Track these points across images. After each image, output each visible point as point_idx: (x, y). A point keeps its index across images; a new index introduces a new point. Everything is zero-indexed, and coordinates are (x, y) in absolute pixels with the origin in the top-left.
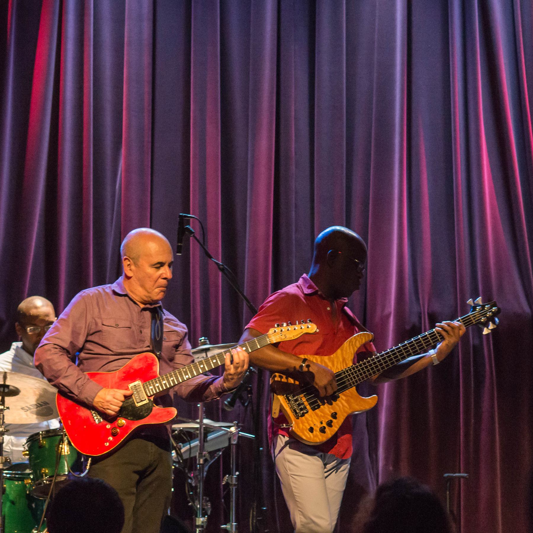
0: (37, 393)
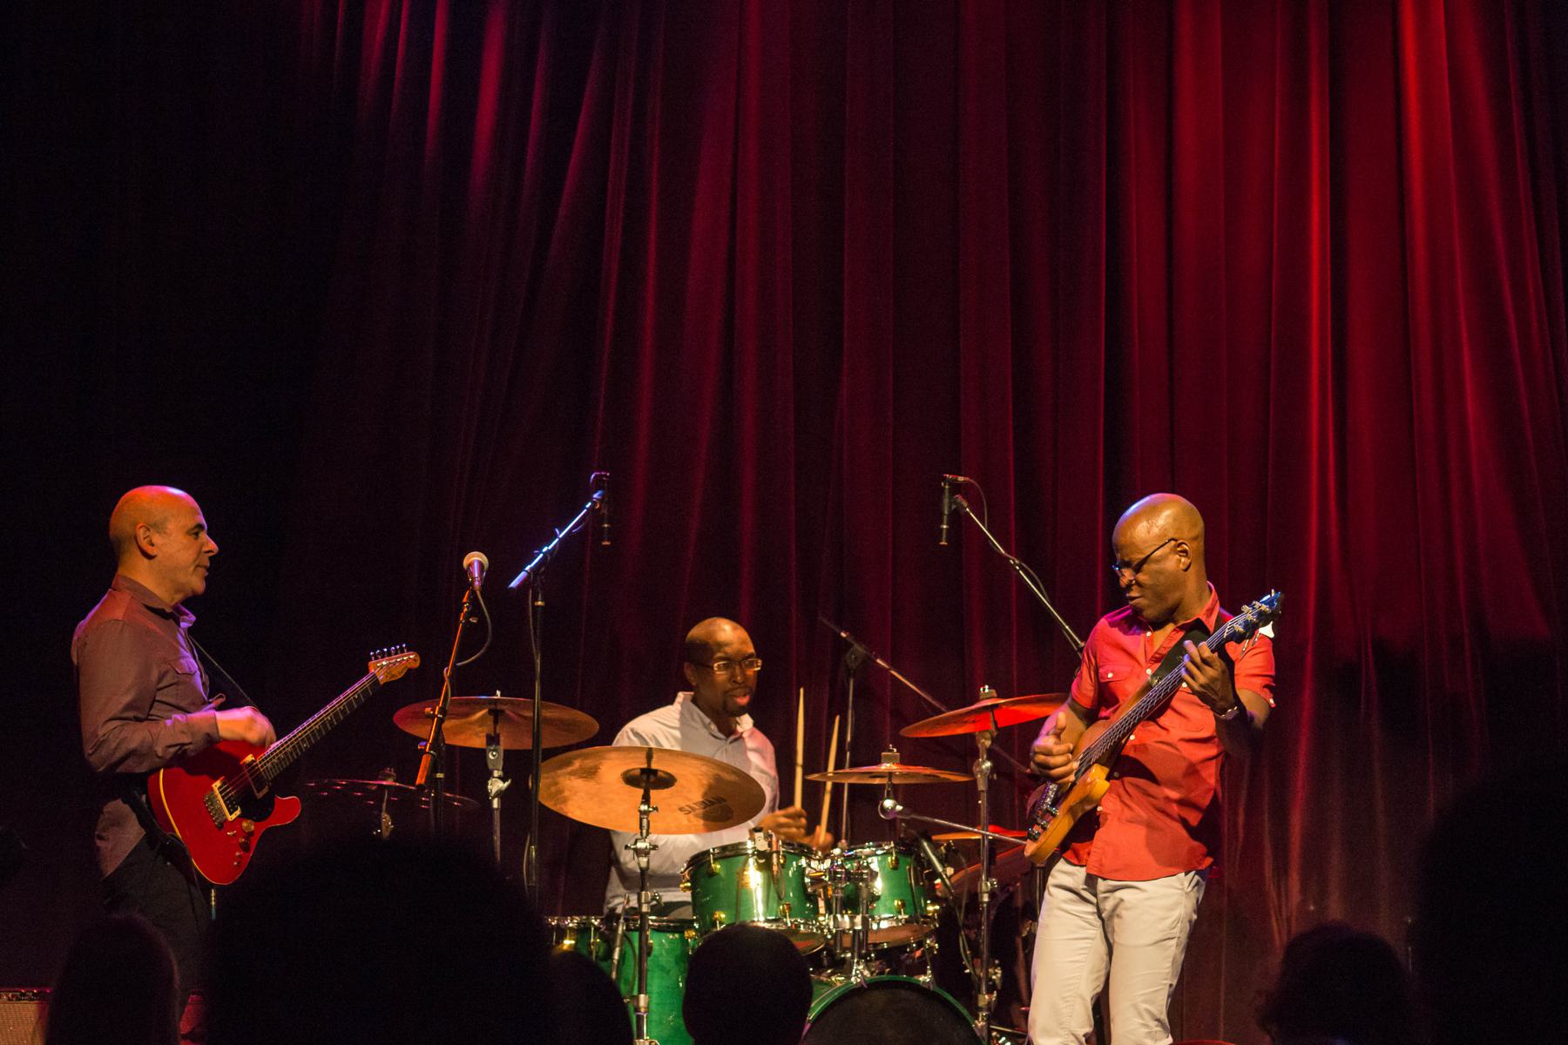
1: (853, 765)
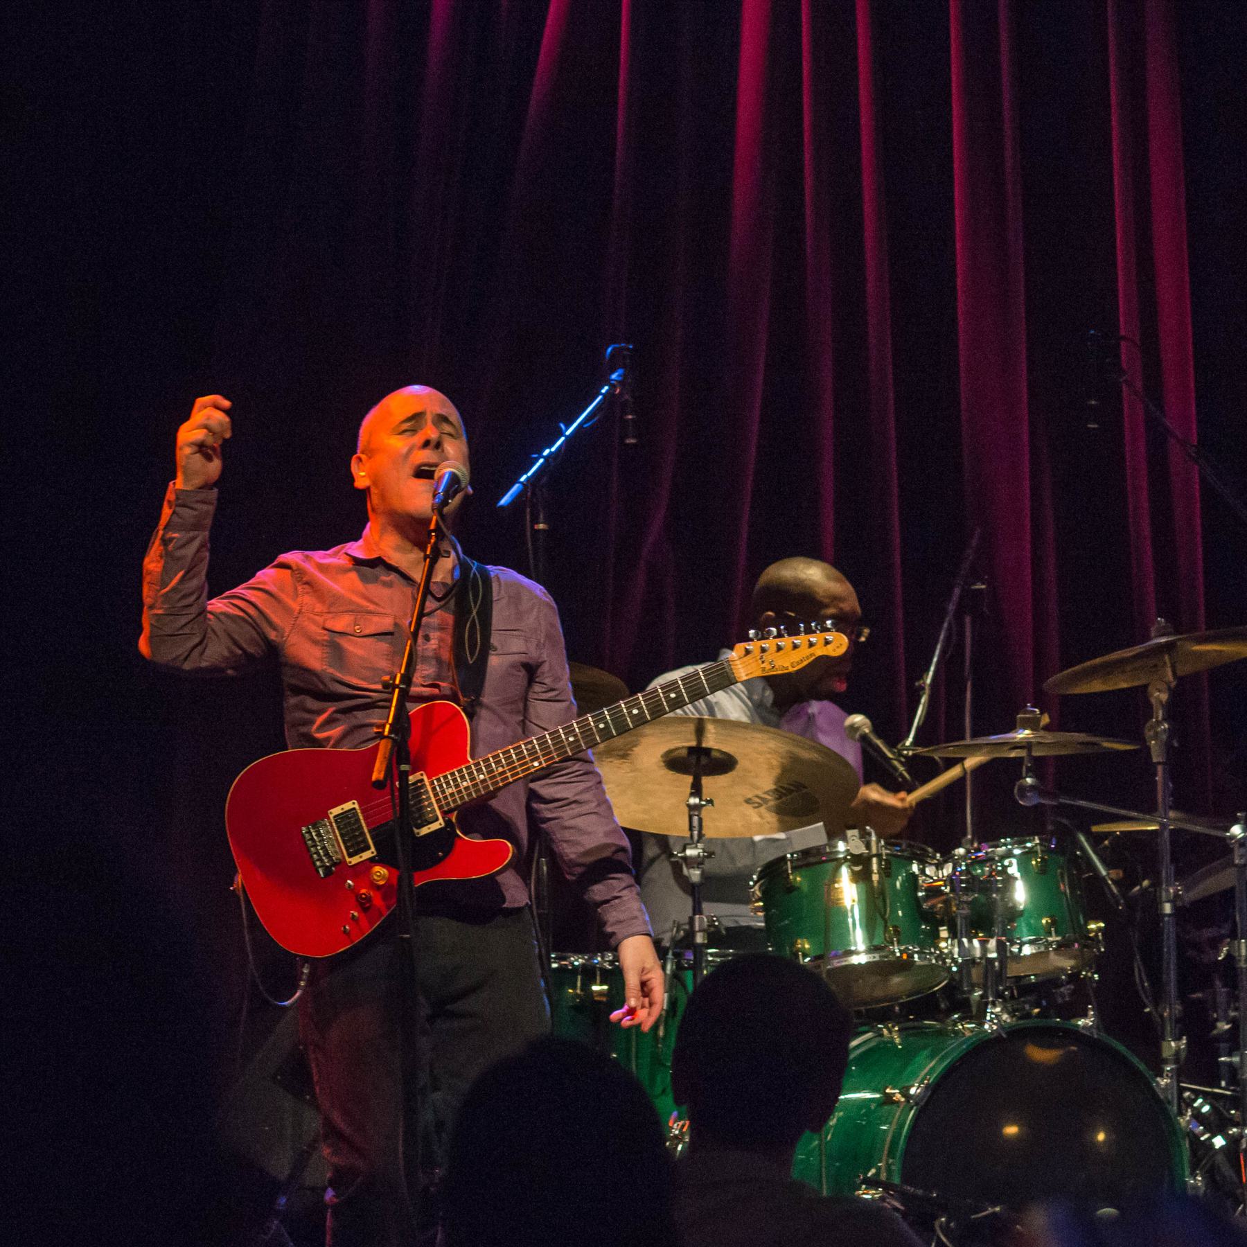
0: (775, 763)
1: (975, 735)
